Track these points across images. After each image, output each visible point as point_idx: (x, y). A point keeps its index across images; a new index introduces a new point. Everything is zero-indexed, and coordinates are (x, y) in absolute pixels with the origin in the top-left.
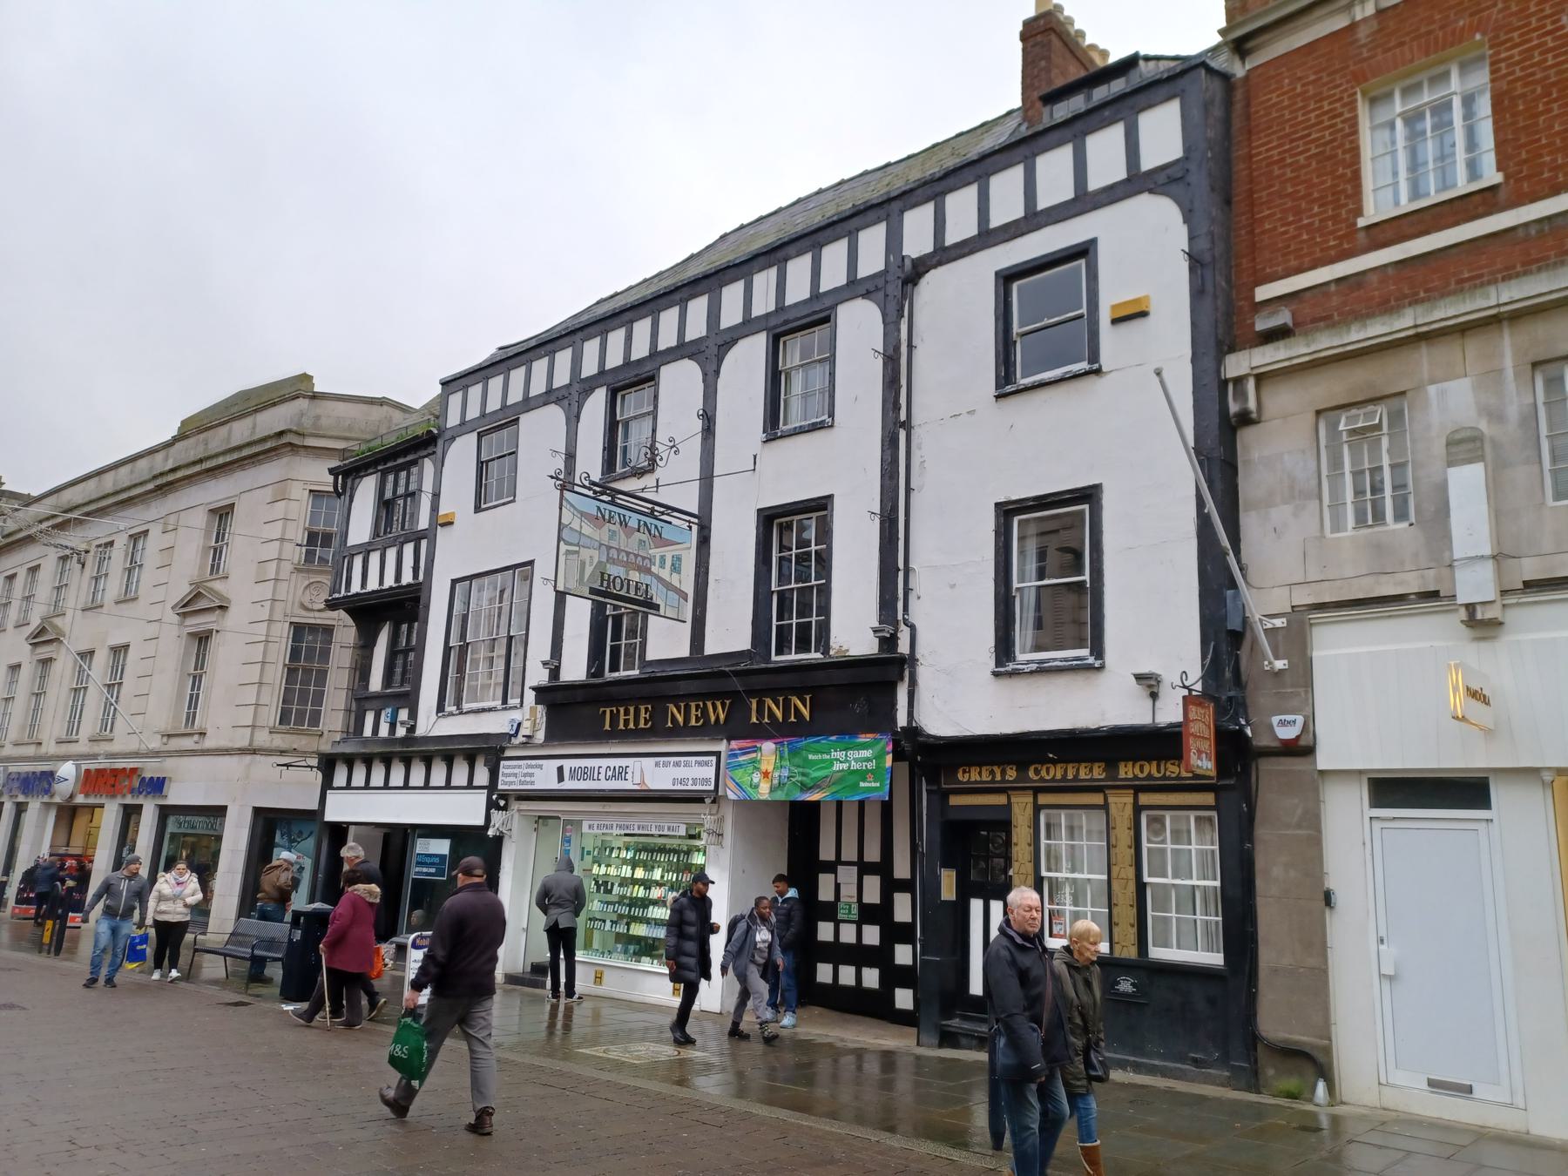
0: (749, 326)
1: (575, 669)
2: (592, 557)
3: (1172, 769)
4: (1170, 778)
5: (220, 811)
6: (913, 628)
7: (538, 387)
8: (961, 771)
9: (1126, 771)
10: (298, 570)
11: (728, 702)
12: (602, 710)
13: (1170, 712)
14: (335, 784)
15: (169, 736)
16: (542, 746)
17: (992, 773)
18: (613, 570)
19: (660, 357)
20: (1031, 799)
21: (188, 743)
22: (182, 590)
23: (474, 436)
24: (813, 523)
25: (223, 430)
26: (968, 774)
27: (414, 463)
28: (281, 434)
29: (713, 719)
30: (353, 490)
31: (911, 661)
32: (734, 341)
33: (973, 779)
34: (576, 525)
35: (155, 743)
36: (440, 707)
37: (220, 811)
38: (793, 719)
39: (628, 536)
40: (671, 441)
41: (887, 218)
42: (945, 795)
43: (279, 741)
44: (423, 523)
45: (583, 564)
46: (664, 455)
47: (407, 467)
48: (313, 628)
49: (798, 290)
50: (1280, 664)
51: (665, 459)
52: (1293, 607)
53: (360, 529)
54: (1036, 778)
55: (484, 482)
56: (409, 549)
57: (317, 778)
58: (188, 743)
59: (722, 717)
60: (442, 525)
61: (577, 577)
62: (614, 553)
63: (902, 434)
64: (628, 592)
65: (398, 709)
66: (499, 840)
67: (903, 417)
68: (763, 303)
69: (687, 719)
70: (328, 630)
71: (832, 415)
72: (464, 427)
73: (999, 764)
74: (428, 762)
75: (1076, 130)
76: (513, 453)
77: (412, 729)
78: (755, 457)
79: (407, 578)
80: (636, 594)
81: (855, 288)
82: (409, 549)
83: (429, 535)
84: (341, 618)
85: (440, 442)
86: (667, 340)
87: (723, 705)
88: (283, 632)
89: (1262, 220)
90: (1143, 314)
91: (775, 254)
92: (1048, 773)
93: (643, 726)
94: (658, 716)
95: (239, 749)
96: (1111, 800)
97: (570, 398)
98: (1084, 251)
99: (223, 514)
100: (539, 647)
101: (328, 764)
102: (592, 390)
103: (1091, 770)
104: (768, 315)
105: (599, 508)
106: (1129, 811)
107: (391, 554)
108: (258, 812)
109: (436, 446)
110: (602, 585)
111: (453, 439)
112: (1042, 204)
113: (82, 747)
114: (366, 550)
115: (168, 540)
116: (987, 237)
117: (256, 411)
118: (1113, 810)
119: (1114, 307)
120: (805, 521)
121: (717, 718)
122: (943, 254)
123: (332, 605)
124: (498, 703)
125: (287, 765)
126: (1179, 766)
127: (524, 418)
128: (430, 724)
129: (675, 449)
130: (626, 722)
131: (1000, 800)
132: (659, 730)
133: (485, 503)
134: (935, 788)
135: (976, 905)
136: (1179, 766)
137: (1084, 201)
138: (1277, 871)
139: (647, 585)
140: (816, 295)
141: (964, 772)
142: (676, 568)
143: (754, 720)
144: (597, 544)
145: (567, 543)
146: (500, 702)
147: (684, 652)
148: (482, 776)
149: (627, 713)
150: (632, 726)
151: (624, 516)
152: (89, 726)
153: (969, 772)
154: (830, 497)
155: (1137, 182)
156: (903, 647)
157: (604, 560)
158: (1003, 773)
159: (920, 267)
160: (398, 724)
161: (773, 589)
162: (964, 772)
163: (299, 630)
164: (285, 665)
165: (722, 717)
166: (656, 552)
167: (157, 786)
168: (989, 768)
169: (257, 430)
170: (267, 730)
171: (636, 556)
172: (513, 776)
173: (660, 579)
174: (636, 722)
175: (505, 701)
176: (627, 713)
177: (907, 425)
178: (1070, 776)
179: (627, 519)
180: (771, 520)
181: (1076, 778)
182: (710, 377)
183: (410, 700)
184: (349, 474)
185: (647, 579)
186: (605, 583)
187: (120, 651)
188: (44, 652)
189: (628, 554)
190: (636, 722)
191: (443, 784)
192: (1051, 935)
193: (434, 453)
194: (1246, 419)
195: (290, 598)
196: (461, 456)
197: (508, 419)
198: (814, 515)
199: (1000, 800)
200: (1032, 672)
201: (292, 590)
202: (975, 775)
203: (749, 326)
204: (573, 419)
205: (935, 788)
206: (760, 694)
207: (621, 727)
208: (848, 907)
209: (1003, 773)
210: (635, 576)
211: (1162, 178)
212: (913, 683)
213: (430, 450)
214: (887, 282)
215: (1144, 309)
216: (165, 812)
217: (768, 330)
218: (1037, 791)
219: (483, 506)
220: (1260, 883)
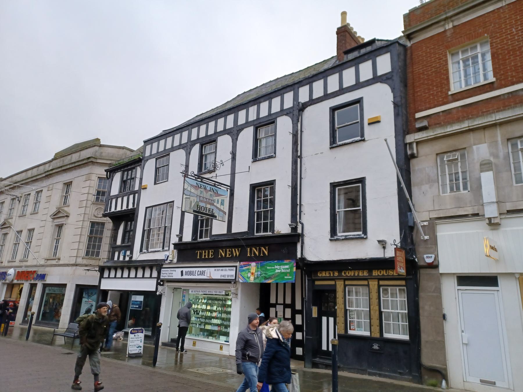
0: (247, 124)
1: (187, 237)
2: (194, 200)
3: (391, 273)
4: (390, 276)
5: (64, 286)
6: (302, 224)
7: (177, 143)
8: (319, 273)
9: (375, 273)
10: (93, 204)
11: (240, 249)
12: (196, 251)
13: (390, 253)
14: (104, 277)
15: (47, 260)
16: (175, 264)
17: (330, 274)
18: (201, 204)
19: (217, 134)
20: (377, 283)
21: (54, 262)
22: (54, 210)
23: (155, 159)
24: (269, 188)
25: (69, 157)
26: (321, 274)
27: (134, 168)
28: (89, 158)
29: (235, 255)
30: (113, 177)
31: (302, 235)
32: (242, 129)
33: (323, 276)
34: (189, 189)
35: (42, 262)
36: (141, 250)
37: (64, 286)
38: (262, 255)
39: (207, 193)
40: (221, 161)
41: (294, 90)
42: (314, 281)
43: (85, 262)
44: (137, 188)
45: (191, 202)
46: (219, 166)
47: (132, 169)
48: (98, 223)
49: (264, 112)
50: (426, 237)
51: (219, 167)
52: (430, 218)
53: (115, 190)
54: (345, 275)
55: (157, 174)
56: (131, 197)
57: (98, 274)
58: (54, 262)
59: (238, 254)
60: (143, 189)
61: (189, 206)
62: (202, 199)
63: (299, 160)
64: (206, 212)
65: (126, 251)
66: (160, 296)
67: (299, 154)
68: (252, 117)
69: (226, 255)
70: (103, 224)
71: (275, 153)
72: (151, 156)
73: (332, 271)
74: (136, 269)
75: (356, 62)
76: (168, 165)
77: (131, 258)
78: (249, 167)
79: (131, 207)
80: (209, 212)
81: (283, 112)
82: (131, 197)
83: (139, 192)
84: (108, 220)
85: (143, 162)
86: (220, 128)
87: (238, 250)
88: (88, 225)
89: (417, 92)
90: (379, 122)
91: (256, 101)
92: (349, 274)
93: (211, 257)
94: (216, 253)
95: (71, 264)
96: (337, 283)
97: (187, 147)
98: (359, 101)
99: (68, 185)
100: (175, 230)
101: (102, 270)
102: (195, 144)
103: (363, 273)
104: (254, 121)
105: (197, 183)
106: (376, 287)
107: (125, 199)
108: (77, 286)
109: (141, 162)
110: (197, 209)
111: (147, 160)
112: (345, 86)
113: (17, 264)
114: (117, 197)
115: (49, 193)
116: (327, 96)
117: (81, 150)
118: (371, 286)
119: (369, 119)
120: (266, 188)
121: (236, 254)
122: (312, 102)
123: (105, 215)
124: (161, 249)
125: (88, 270)
126: (393, 272)
127: (172, 154)
128: (137, 256)
129: (222, 164)
130: (205, 256)
131: (332, 283)
132: (216, 258)
133: (158, 182)
134: (310, 278)
135: (324, 319)
136: (393, 272)
137: (359, 85)
138: (427, 307)
139: (213, 209)
140: (270, 114)
141: (320, 273)
142: (222, 204)
143: (249, 255)
144: (196, 195)
145: (186, 195)
146: (162, 249)
147: (225, 232)
148: (155, 274)
149: (205, 252)
150: (207, 257)
151: (205, 186)
152: (20, 256)
153: (322, 273)
154: (275, 180)
155: (376, 79)
156: (299, 231)
157: (198, 200)
158: (333, 274)
159: (305, 106)
160: (126, 256)
161: (255, 211)
162: (320, 273)
163: (93, 224)
164: (88, 236)
165: (238, 254)
166: (216, 198)
167: (43, 277)
168: (329, 272)
169: (81, 157)
170: (81, 258)
171: (209, 199)
172: (165, 274)
173: (217, 207)
174: (208, 256)
175: (163, 248)
176: (205, 252)
177: (300, 157)
178: (356, 275)
179: (206, 187)
180: (255, 188)
181: (333, 276)
182: (235, 141)
183: (131, 248)
184: (111, 171)
185: (212, 207)
186: (198, 208)
187: (31, 231)
188: (4, 231)
189: (206, 199)
190: (208, 256)
191: (149, 277)
192: (350, 329)
193: (141, 165)
194: (413, 156)
195: (90, 213)
196: (150, 166)
197: (166, 154)
198: (269, 186)
199: (332, 283)
200: (343, 239)
201: (91, 210)
202: (324, 274)
203: (247, 124)
204: (188, 154)
205: (310, 278)
206: (251, 246)
207: (203, 257)
208: (280, 319)
209: (333, 274)
210: (209, 206)
211: (384, 78)
212: (303, 243)
213: (139, 164)
214: (293, 110)
215: (379, 120)
216: (45, 286)
217: (254, 125)
218: (345, 280)
219: (157, 183)
220: (421, 311)
